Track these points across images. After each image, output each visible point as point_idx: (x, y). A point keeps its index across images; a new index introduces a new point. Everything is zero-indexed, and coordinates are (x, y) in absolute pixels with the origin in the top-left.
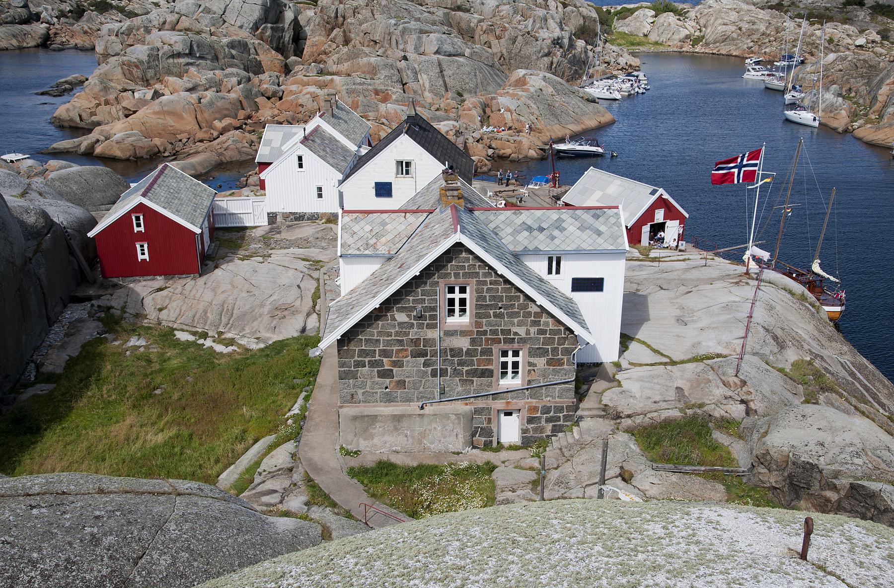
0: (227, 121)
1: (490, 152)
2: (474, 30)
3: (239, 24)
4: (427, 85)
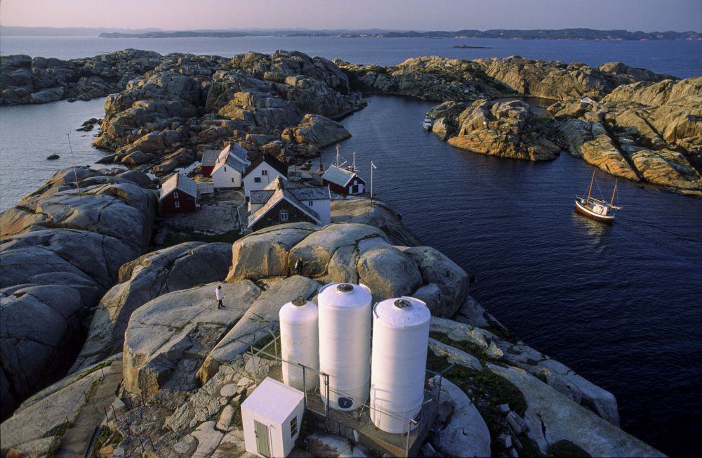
0: (178, 144)
1: (296, 154)
2: (287, 92)
3: (174, 92)
4: (267, 122)
